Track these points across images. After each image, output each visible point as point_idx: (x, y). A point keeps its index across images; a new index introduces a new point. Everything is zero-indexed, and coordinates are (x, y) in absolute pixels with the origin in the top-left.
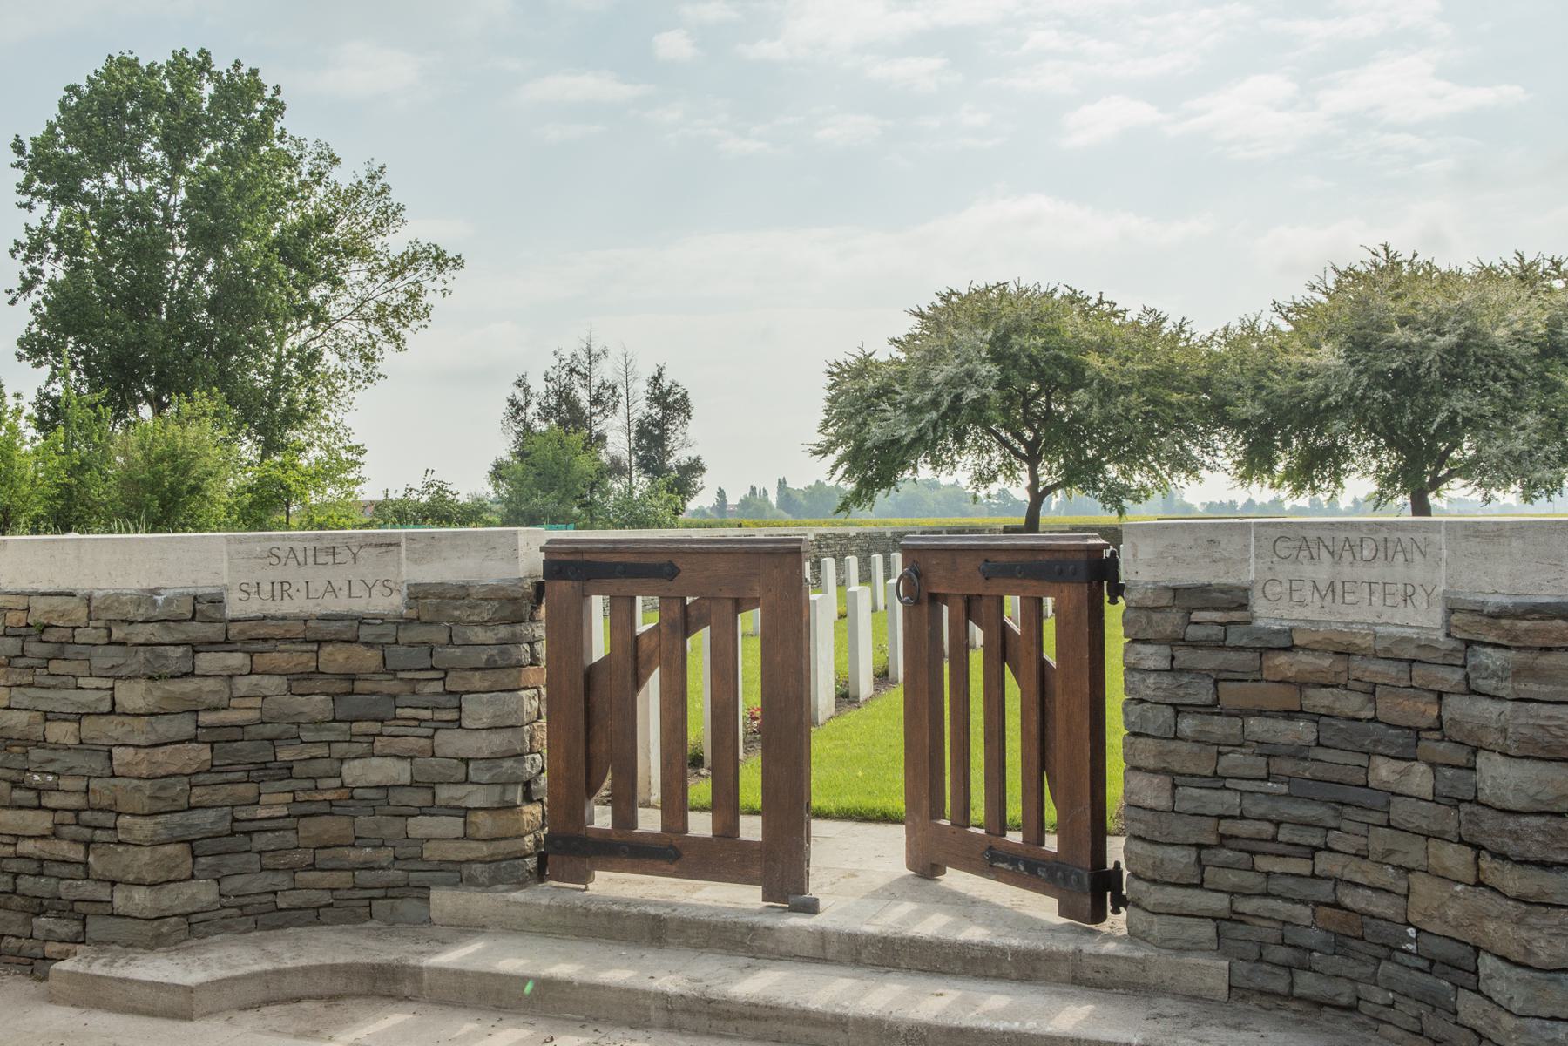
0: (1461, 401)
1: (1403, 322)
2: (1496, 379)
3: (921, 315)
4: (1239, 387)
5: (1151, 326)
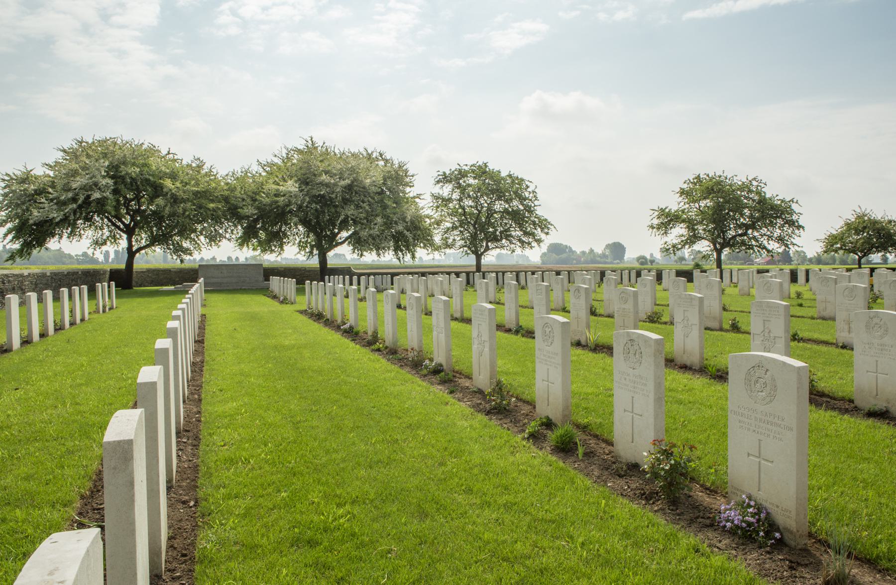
0: (350, 211)
1: (326, 173)
2: (363, 202)
3: (64, 151)
4: (243, 200)
5: (198, 166)
